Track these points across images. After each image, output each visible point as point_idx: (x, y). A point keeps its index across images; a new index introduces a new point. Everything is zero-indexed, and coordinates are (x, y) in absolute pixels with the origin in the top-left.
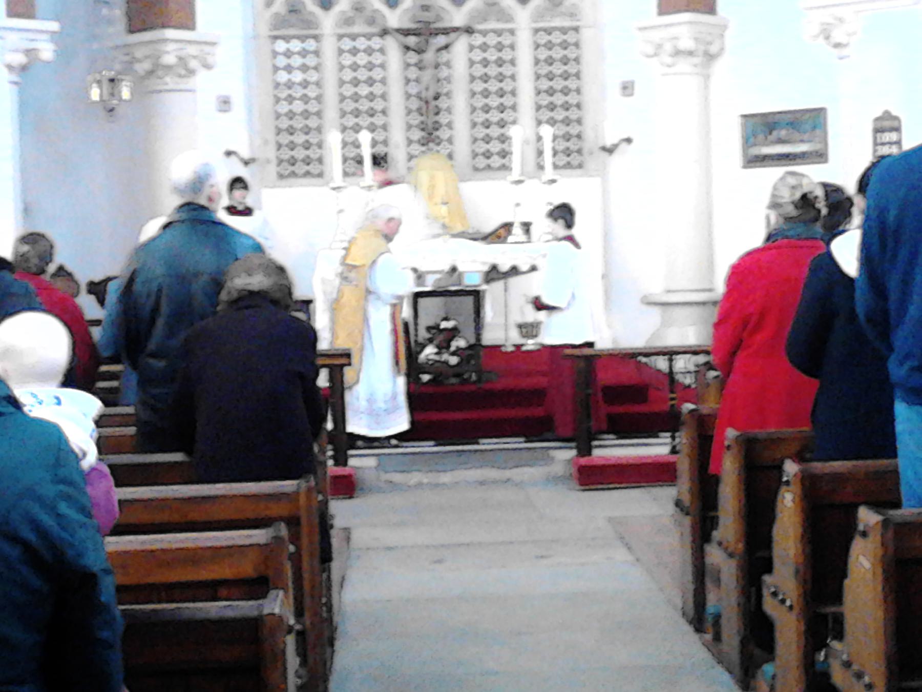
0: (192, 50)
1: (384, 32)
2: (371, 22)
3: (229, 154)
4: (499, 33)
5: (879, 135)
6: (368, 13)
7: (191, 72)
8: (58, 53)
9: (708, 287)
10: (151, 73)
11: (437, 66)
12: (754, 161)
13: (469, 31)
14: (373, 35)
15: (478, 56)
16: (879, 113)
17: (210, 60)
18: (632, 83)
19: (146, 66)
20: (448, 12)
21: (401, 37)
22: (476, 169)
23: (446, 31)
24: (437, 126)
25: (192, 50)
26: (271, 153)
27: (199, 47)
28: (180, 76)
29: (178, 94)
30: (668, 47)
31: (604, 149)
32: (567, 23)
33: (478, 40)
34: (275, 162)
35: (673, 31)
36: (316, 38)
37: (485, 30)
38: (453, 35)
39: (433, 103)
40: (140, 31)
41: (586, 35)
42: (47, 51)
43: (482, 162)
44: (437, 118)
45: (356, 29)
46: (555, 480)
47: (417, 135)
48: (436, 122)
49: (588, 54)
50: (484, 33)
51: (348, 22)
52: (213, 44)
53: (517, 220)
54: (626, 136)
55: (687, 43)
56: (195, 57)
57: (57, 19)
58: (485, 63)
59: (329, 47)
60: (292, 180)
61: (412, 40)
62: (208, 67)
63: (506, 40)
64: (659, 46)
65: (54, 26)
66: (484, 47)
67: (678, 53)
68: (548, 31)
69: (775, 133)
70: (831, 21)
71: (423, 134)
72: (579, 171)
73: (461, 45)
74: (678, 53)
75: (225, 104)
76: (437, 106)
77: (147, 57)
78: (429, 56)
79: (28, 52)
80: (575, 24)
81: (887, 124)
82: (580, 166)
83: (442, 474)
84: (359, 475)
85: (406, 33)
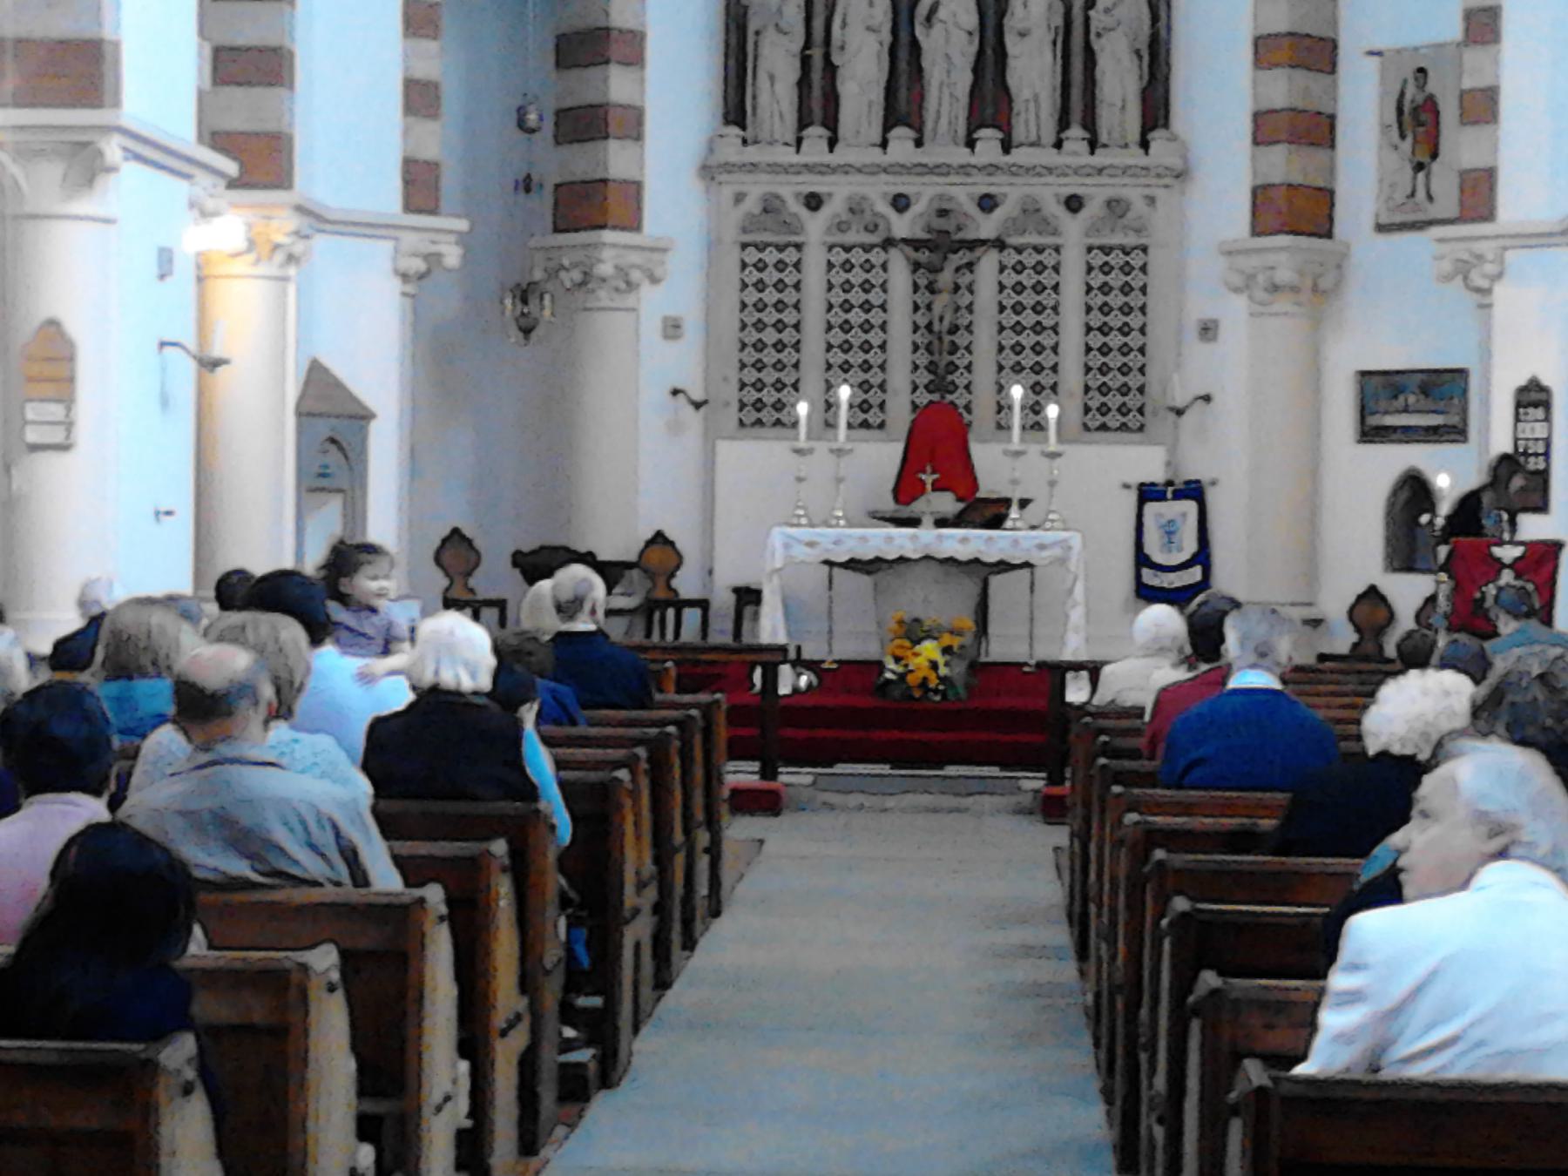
0: (635, 258)
1: (888, 243)
2: (872, 228)
3: (675, 392)
4: (1039, 250)
5: (1521, 410)
6: (868, 216)
7: (631, 286)
8: (465, 258)
9: (1307, 601)
10: (583, 284)
11: (957, 288)
12: (1370, 433)
13: (1000, 244)
14: (873, 246)
15: (1010, 278)
16: (1523, 382)
17: (658, 272)
18: (1216, 323)
19: (577, 275)
20: (973, 219)
21: (909, 250)
22: (1086, 428)
23: (973, 245)
24: (952, 367)
25: (635, 258)
26: (731, 393)
27: (648, 254)
28: (617, 290)
29: (611, 313)
30: (1261, 279)
31: (1172, 409)
32: (1130, 240)
33: (1011, 258)
34: (736, 406)
35: (1271, 259)
36: (798, 247)
37: (1022, 245)
38: (979, 251)
39: (947, 338)
40: (567, 231)
41: (1156, 258)
42: (452, 256)
43: (1095, 420)
44: (953, 358)
45: (851, 237)
46: (1020, 811)
47: (960, 379)
48: (952, 363)
49: (1158, 280)
50: (1019, 250)
51: (842, 227)
52: (664, 250)
53: (1016, 495)
54: (1202, 393)
55: (1284, 275)
56: (638, 267)
57: (467, 216)
58: (1019, 288)
59: (814, 260)
60: (757, 430)
61: (924, 256)
62: (654, 280)
63: (1049, 258)
64: (1251, 278)
65: (462, 225)
66: (1019, 268)
67: (1275, 288)
68: (1106, 250)
69: (1401, 398)
70: (1466, 256)
71: (932, 377)
72: (1136, 437)
73: (988, 263)
74: (1275, 288)
75: (672, 329)
76: (953, 343)
77: (575, 265)
78: (946, 278)
79: (427, 257)
80: (1143, 241)
81: (1534, 396)
82: (1141, 428)
83: (887, 798)
84: (785, 793)
85: (915, 244)
